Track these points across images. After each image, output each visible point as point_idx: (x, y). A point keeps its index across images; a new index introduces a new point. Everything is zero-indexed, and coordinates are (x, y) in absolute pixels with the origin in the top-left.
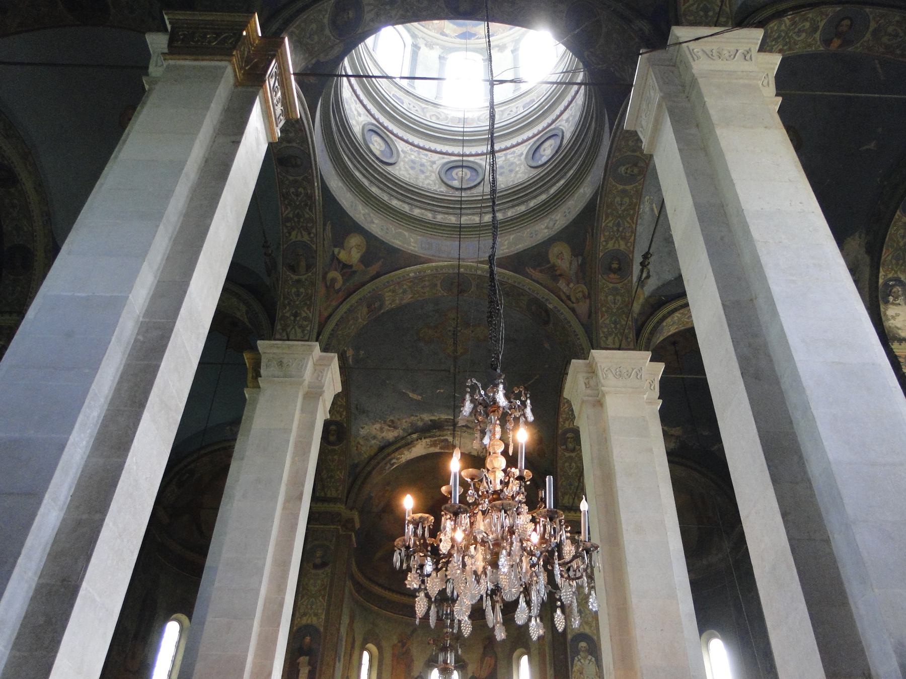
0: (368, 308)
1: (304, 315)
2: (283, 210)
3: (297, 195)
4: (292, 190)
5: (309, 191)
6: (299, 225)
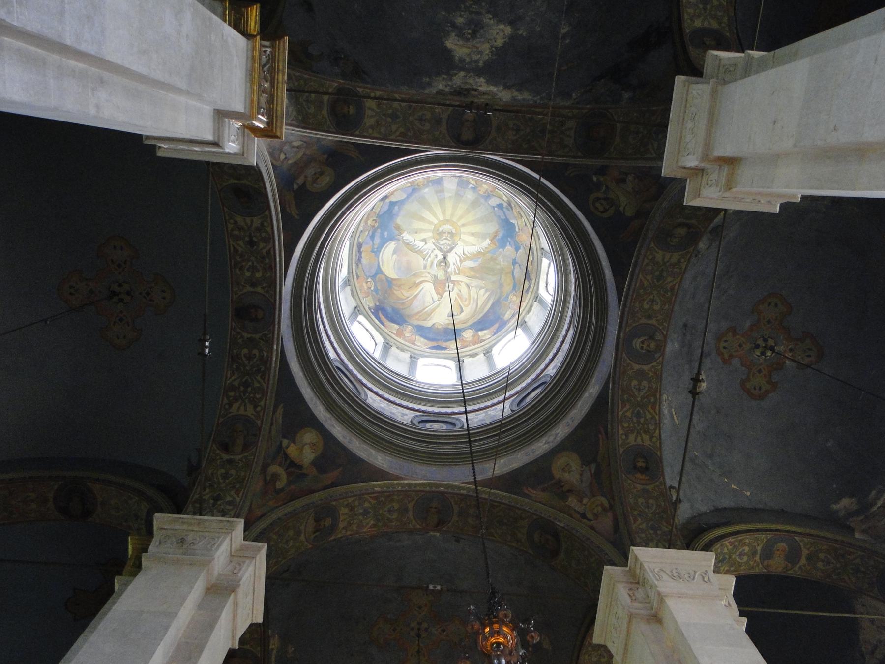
0: (315, 521)
1: (229, 498)
2: (229, 375)
3: (250, 357)
4: (245, 351)
5: (265, 354)
6: (244, 395)
